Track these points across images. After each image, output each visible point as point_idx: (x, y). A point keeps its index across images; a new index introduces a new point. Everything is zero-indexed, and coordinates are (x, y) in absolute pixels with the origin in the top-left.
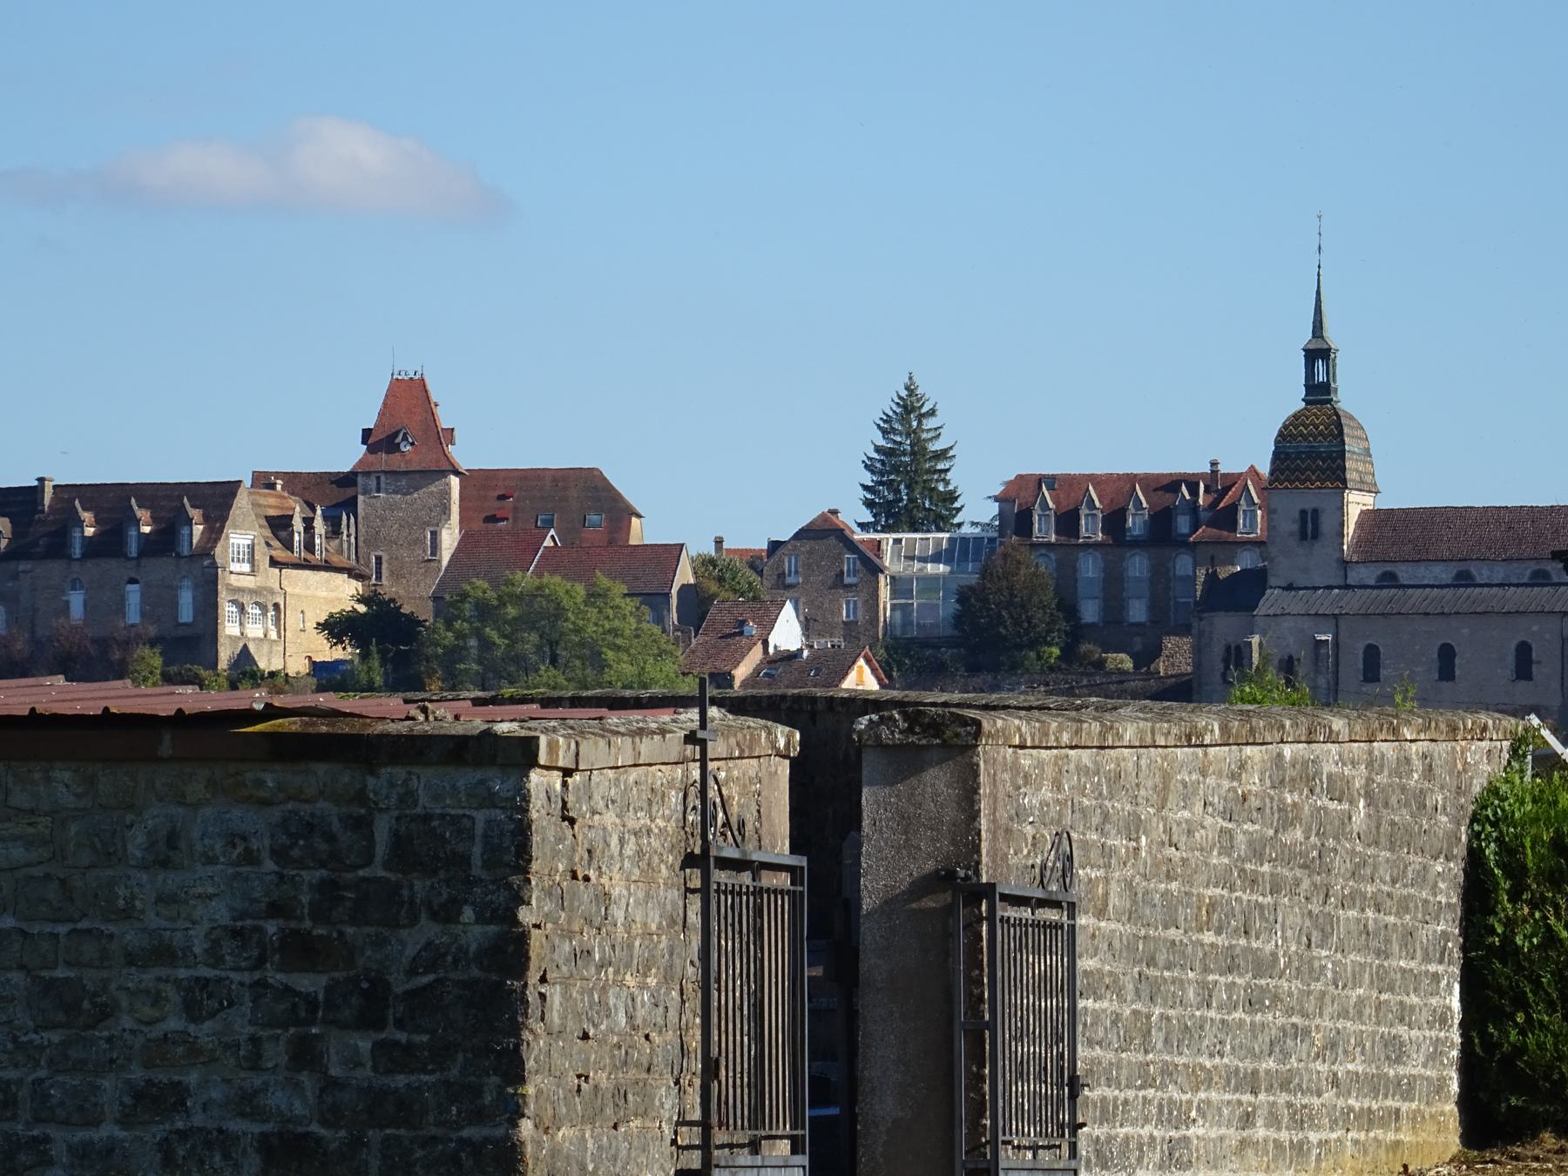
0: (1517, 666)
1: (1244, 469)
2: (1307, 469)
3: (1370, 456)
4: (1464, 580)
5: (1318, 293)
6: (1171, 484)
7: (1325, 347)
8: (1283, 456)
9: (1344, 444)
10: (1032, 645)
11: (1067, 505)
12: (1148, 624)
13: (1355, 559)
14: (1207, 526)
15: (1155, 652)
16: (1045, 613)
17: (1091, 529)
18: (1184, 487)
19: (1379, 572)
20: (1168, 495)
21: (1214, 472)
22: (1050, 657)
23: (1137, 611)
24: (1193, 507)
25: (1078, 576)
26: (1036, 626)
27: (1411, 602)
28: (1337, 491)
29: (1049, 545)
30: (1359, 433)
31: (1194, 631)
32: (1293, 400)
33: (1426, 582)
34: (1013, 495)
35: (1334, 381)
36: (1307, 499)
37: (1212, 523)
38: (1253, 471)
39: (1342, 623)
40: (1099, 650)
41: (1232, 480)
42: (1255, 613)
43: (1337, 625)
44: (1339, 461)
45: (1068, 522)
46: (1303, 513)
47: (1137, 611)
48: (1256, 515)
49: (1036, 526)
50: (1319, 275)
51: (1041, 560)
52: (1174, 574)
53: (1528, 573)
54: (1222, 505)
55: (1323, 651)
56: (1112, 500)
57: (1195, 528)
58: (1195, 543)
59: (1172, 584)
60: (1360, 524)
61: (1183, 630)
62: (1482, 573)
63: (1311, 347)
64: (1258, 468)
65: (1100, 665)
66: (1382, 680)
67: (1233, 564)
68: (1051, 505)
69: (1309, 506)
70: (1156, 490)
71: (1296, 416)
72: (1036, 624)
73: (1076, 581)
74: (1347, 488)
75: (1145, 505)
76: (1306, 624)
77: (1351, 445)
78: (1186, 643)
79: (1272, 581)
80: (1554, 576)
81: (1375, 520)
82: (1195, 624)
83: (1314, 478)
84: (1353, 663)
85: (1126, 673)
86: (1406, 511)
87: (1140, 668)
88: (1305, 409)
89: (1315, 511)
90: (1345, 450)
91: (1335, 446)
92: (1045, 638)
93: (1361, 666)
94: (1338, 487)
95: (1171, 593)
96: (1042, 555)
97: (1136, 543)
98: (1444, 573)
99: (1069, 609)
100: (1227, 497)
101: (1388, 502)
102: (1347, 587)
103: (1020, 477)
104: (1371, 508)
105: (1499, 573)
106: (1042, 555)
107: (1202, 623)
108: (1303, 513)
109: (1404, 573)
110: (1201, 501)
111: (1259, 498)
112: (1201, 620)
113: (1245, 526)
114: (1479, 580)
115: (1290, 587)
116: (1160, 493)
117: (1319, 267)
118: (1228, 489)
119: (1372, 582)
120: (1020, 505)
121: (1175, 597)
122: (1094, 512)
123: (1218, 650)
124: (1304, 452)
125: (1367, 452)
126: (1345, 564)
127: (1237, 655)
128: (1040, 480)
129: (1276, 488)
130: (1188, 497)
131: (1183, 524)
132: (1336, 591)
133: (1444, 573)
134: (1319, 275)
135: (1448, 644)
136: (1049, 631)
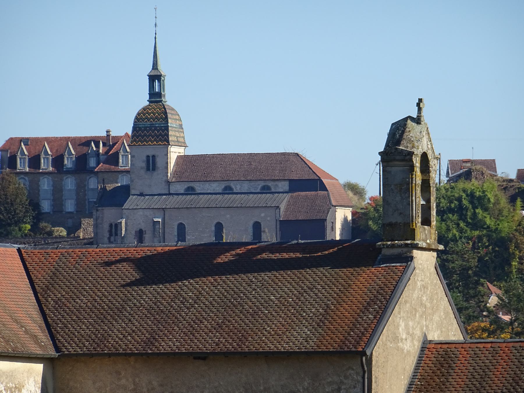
0: (254, 234)
1: (122, 134)
2: (149, 136)
3: (182, 129)
4: (228, 190)
5: (155, 47)
6: (86, 142)
7: (159, 74)
8: (138, 129)
9: (168, 123)
10: (17, 223)
11: (34, 153)
12: (51, 213)
13: (173, 180)
14: (103, 163)
15: (78, 227)
16: (23, 207)
17: (46, 165)
18: (92, 143)
19: (186, 187)
20: (85, 148)
21: (108, 136)
22: (25, 230)
23: (70, 206)
24: (97, 154)
25: (40, 188)
26: (18, 214)
27: (201, 202)
28: (165, 146)
29: (26, 173)
30: (177, 117)
31: (94, 217)
32: (143, 101)
33: (209, 192)
34: (7, 148)
35: (164, 91)
36: (150, 150)
37: (106, 162)
38: (127, 134)
39: (166, 212)
40: (50, 226)
41: (117, 139)
42: (123, 208)
43: (164, 215)
44: (166, 131)
45: (35, 161)
46: (148, 157)
47: (70, 206)
48: (128, 158)
49: (121, 161)
50: (155, 38)
51: (21, 181)
52: (88, 187)
53: (260, 187)
54: (111, 152)
55: (157, 227)
56: (57, 150)
57: (98, 164)
58: (97, 172)
59: (87, 192)
60: (177, 163)
61: (90, 216)
62: (237, 187)
63: (152, 74)
64: (129, 133)
65: (50, 233)
66: (186, 241)
67: (117, 183)
68: (26, 153)
69: (150, 154)
70: (79, 145)
71: (144, 109)
72: (18, 213)
73: (39, 191)
74: (169, 145)
75: (26, 153)
76: (148, 213)
77: (171, 123)
78: (91, 221)
79: (133, 192)
80: (273, 189)
81: (183, 160)
82: (94, 213)
83: (158, 139)
84: (147, 237)
85: (63, 237)
86: (213, 156)
87: (71, 235)
88: (149, 105)
89: (154, 156)
90: (168, 126)
91: (163, 124)
92: (23, 220)
93: (176, 234)
94: (165, 145)
95: (87, 197)
96: (22, 178)
97: (69, 172)
98: (218, 187)
99: (35, 205)
100: (114, 148)
101: (192, 151)
102: (170, 194)
103: (11, 139)
104: (183, 154)
105: (245, 187)
106: (22, 178)
107: (98, 213)
108: (148, 157)
109: (199, 187)
110: (101, 151)
111: (51, 152)
112: (97, 210)
113: (123, 163)
114: (235, 191)
115: (141, 195)
116: (81, 147)
117: (156, 34)
118: (114, 144)
119: (182, 192)
120: (11, 153)
121: (88, 199)
122: (48, 156)
123: (106, 227)
124: (148, 127)
125: (181, 126)
126: (168, 183)
127: (115, 229)
128: (21, 140)
129: (135, 145)
130: (95, 149)
131: (92, 162)
132: (165, 196)
133: (218, 187)
134: (155, 38)
135: (221, 223)
136: (25, 216)
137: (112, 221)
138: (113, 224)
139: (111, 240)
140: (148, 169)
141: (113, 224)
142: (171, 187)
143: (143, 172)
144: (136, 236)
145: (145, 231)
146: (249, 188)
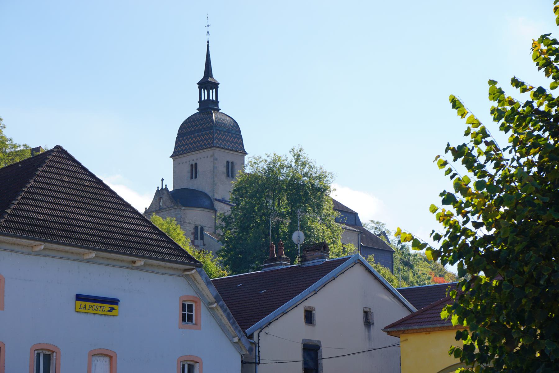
50: (208, 46)
69: (230, 160)
89: (232, 163)
108: (228, 162)
117: (208, 42)
134: (208, 46)
137: (197, 223)
139: (196, 244)
140: (228, 175)
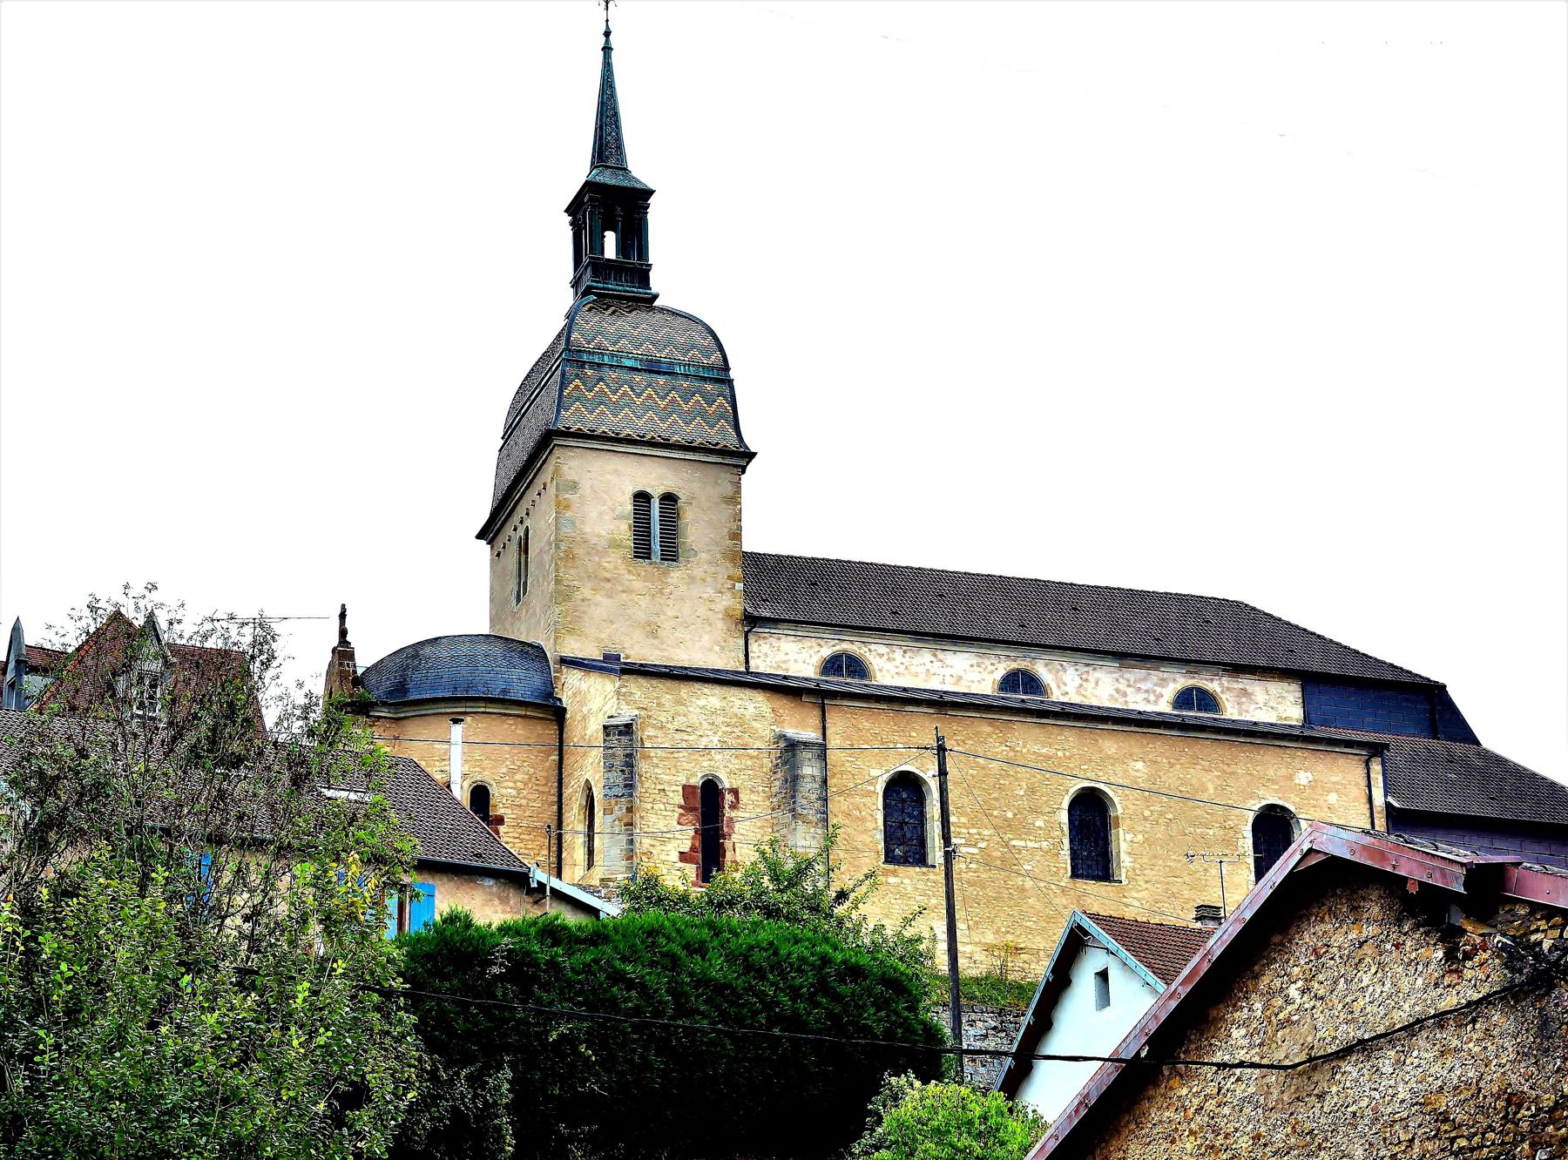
19: (827, 651)
46: (642, 498)
50: (607, 49)
117: (607, 34)
134: (607, 49)
138: (656, 557)
140: (642, 551)
141: (656, 557)
142: (753, 647)
143: (617, 562)
144: (687, 808)
145: (735, 792)
146: (1117, 691)
